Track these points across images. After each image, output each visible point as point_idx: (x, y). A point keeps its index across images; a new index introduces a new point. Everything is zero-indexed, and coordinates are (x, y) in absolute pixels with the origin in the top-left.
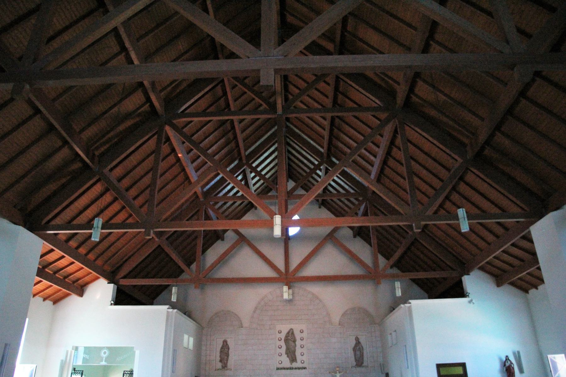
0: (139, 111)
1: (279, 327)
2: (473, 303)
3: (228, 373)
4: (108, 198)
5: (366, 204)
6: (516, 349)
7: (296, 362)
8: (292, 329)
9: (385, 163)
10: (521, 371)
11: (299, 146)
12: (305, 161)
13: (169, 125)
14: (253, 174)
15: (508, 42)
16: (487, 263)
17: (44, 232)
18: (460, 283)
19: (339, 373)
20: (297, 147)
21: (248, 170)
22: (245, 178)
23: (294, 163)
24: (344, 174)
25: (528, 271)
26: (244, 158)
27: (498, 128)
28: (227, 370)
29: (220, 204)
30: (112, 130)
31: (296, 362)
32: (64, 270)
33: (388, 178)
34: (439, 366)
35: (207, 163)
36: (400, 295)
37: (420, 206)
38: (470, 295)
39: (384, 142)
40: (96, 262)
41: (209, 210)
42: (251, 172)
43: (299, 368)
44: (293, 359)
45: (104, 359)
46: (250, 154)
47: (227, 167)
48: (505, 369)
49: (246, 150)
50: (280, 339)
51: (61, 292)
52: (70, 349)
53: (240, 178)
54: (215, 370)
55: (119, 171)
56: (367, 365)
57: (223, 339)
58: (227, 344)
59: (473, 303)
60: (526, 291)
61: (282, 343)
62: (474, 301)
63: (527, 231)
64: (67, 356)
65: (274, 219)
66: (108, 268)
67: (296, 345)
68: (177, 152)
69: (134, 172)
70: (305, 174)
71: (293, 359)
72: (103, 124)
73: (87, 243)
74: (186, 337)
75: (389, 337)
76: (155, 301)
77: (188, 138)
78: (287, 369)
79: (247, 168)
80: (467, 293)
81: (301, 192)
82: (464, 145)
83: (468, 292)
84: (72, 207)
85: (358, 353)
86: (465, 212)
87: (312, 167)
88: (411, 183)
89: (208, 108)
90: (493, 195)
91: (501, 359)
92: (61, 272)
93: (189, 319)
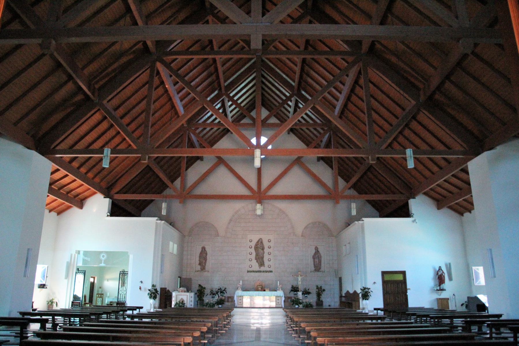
0: (134, 49)
1: (250, 237)
2: (416, 223)
3: (205, 274)
4: (105, 125)
5: (330, 134)
6: (448, 262)
7: (264, 267)
8: (261, 239)
9: (348, 99)
10: (450, 279)
11: (272, 79)
12: (278, 92)
13: (160, 62)
14: (230, 103)
15: (457, 17)
16: (431, 189)
17: (53, 156)
18: (407, 204)
19: (301, 276)
20: (271, 80)
21: (226, 100)
22: (223, 106)
23: (266, 92)
24: (314, 109)
25: (464, 198)
26: (223, 89)
27: (448, 77)
28: (205, 271)
29: (200, 129)
30: (110, 65)
31: (264, 267)
32: (59, 182)
33: (351, 112)
34: (384, 273)
35: (191, 93)
36: (355, 214)
37: (377, 138)
38: (414, 216)
39: (349, 81)
40: (94, 180)
41: (192, 135)
42: (229, 101)
43: (266, 272)
44: (262, 264)
45: (103, 261)
46: (229, 84)
47: (207, 97)
48: (437, 277)
49: (225, 81)
50: (251, 247)
51: (64, 205)
52: (74, 253)
53: (219, 106)
54: (195, 271)
55: (116, 102)
56: (324, 271)
57: (202, 246)
58: (205, 250)
59: (416, 223)
60: (462, 214)
61: (253, 250)
62: (417, 221)
63: (466, 165)
65: (255, 152)
66: (104, 184)
67: (264, 252)
68: (166, 84)
69: (128, 102)
70: (277, 104)
71: (262, 264)
72: (101, 61)
73: (87, 164)
74: (171, 243)
75: (344, 247)
76: (143, 212)
77: (174, 72)
78: (257, 272)
79: (226, 98)
80: (412, 214)
81: (273, 120)
82: (418, 89)
83: (413, 213)
84: (75, 134)
85: (317, 260)
86: (412, 152)
87: (284, 98)
88: (370, 116)
90: (441, 133)
91: (435, 269)
92: (72, 192)
93: (173, 228)
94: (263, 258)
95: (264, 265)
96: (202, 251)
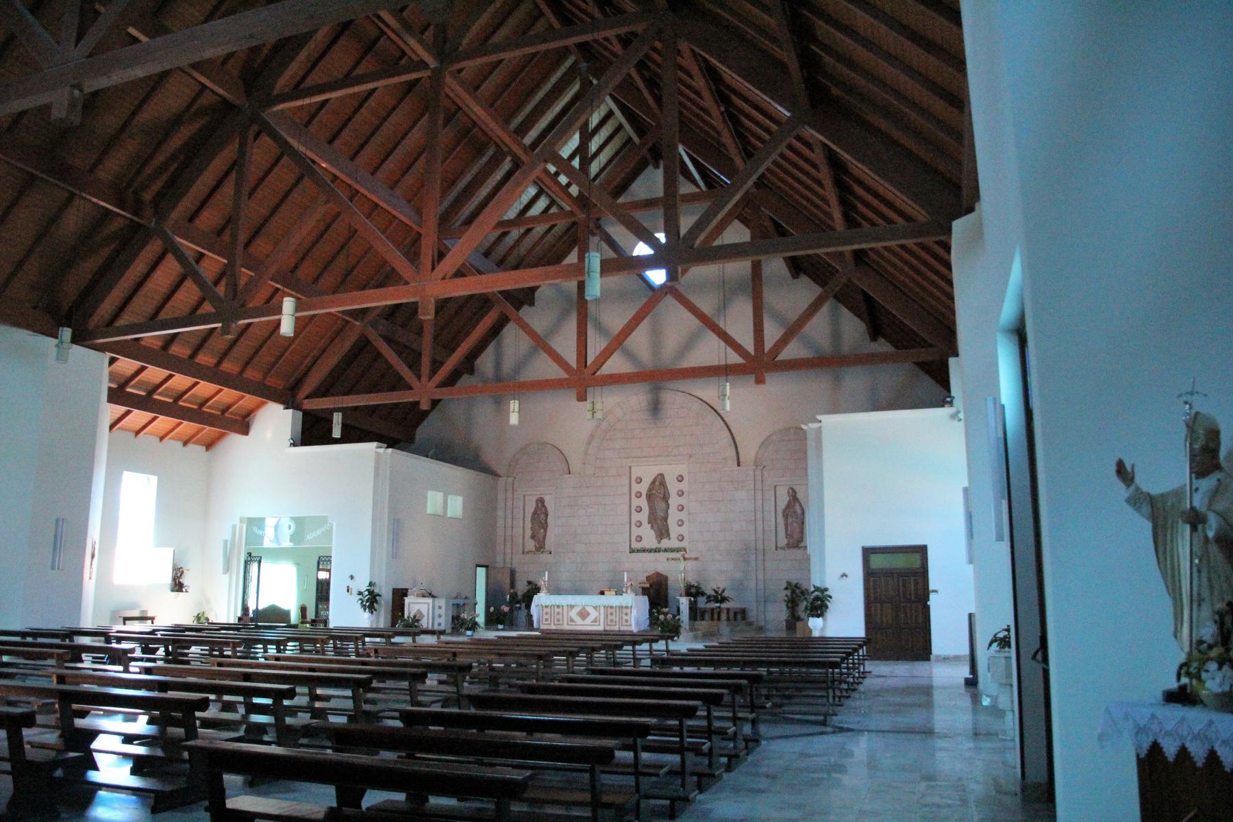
3: (544, 557)
34: (868, 552)
44: (663, 533)
52: (237, 522)
57: (538, 496)
58: (543, 505)
61: (643, 502)
64: (234, 535)
67: (668, 505)
71: (663, 533)
72: (130, 146)
78: (650, 551)
89: (354, 68)
94: (665, 519)
95: (669, 535)
96: (537, 508)
